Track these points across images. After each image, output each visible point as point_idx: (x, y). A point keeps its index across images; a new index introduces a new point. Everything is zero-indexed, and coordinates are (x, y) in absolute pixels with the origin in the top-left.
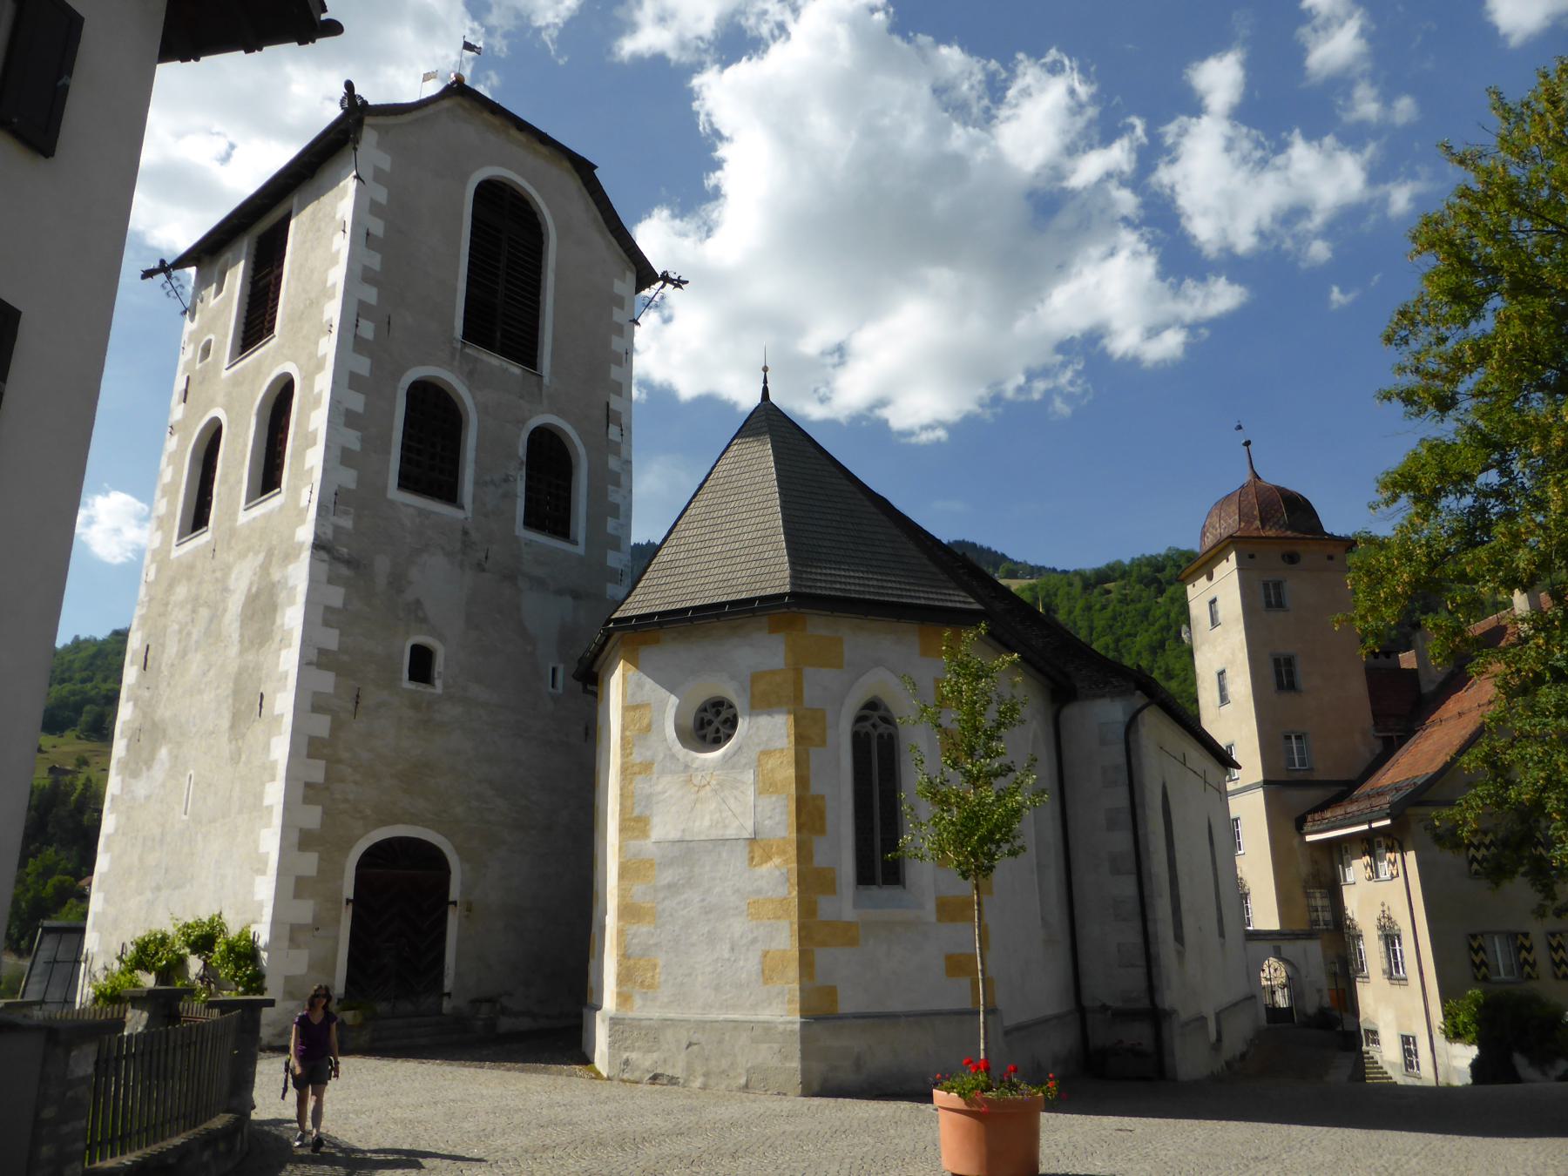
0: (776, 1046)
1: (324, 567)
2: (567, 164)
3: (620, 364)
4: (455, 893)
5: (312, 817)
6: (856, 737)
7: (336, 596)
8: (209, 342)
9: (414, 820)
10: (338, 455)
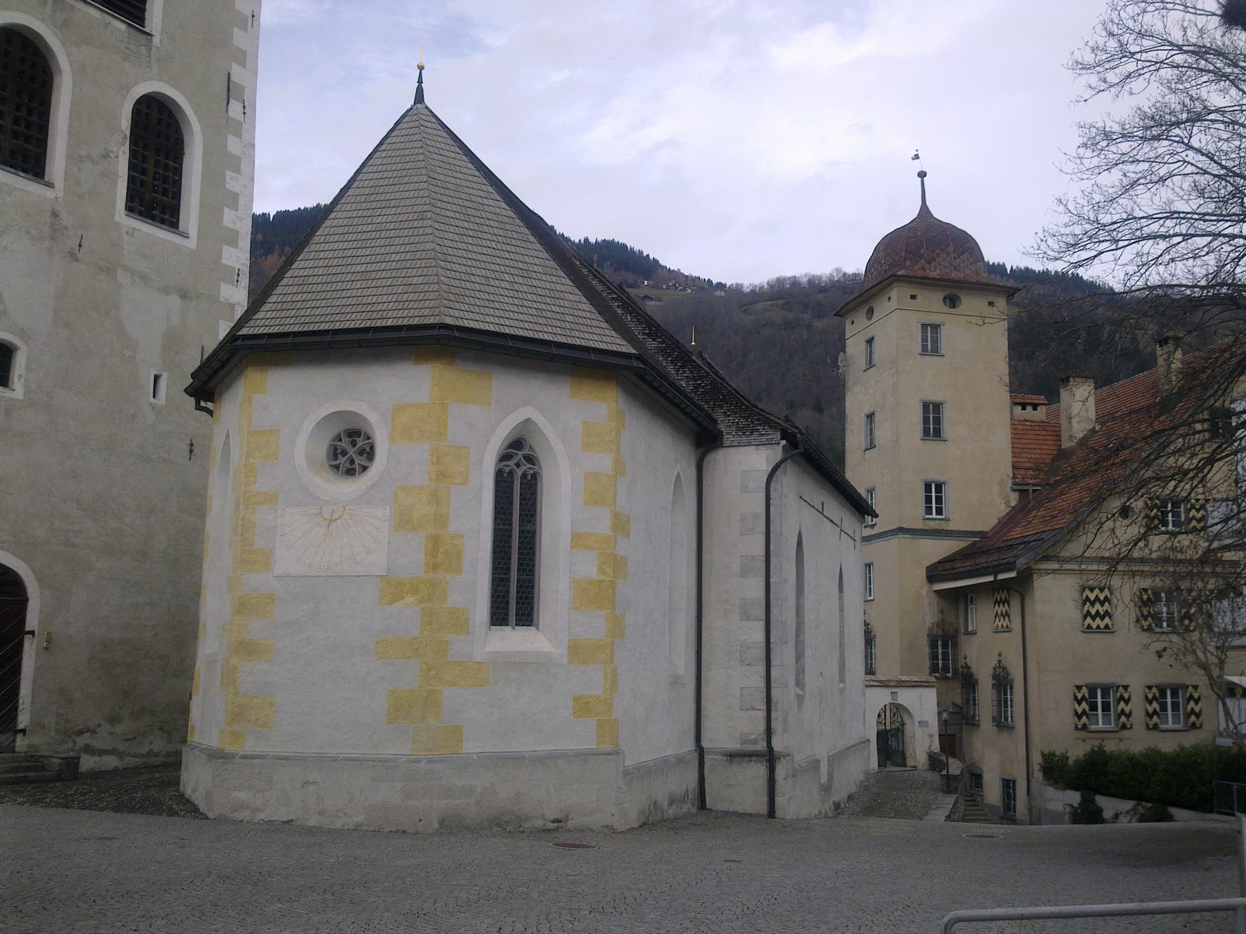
3: (244, 28)
6: (499, 474)
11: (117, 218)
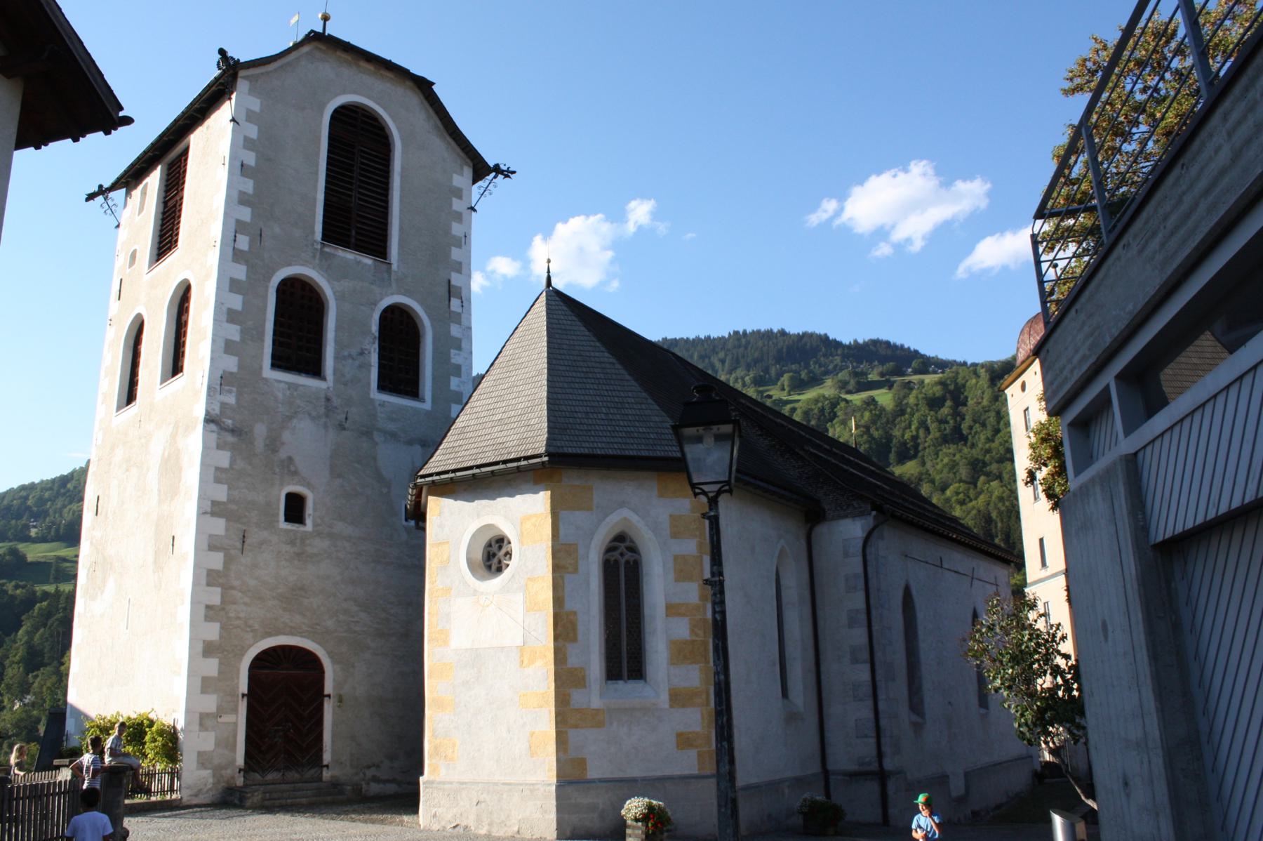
0: (539, 803)
1: (214, 436)
2: (409, 83)
4: (329, 688)
5: (213, 632)
7: (224, 459)
8: (135, 251)
9: (292, 632)
10: (223, 346)
11: (372, 396)
